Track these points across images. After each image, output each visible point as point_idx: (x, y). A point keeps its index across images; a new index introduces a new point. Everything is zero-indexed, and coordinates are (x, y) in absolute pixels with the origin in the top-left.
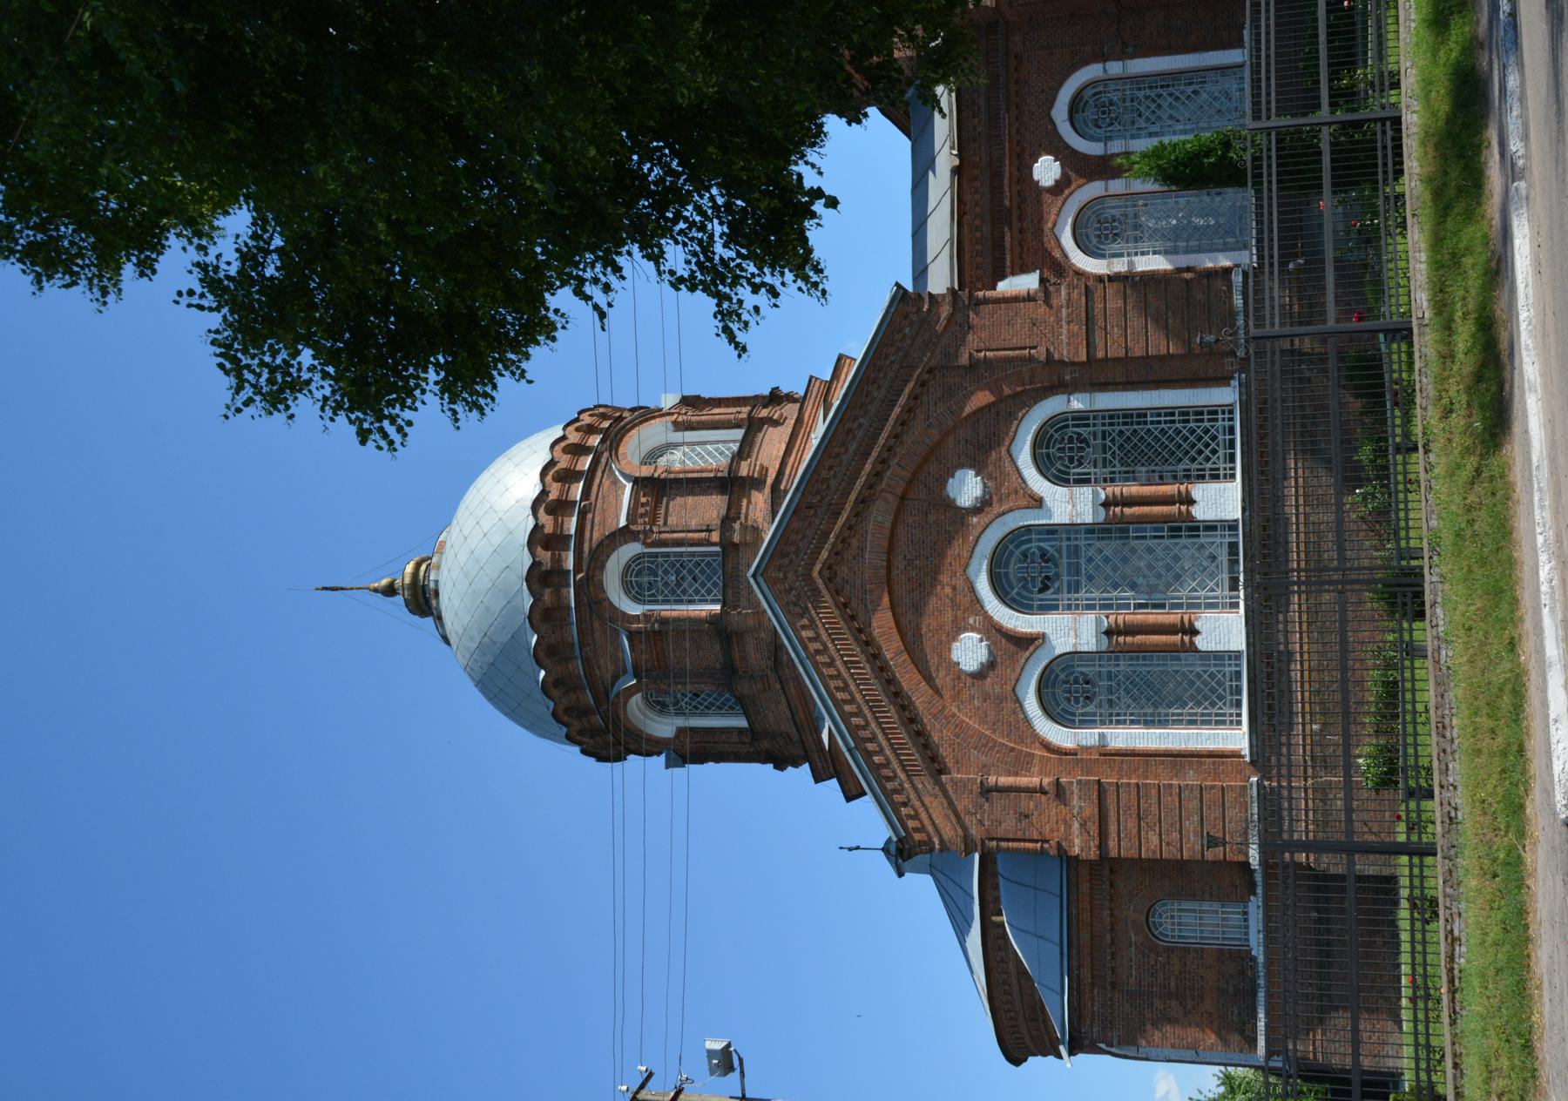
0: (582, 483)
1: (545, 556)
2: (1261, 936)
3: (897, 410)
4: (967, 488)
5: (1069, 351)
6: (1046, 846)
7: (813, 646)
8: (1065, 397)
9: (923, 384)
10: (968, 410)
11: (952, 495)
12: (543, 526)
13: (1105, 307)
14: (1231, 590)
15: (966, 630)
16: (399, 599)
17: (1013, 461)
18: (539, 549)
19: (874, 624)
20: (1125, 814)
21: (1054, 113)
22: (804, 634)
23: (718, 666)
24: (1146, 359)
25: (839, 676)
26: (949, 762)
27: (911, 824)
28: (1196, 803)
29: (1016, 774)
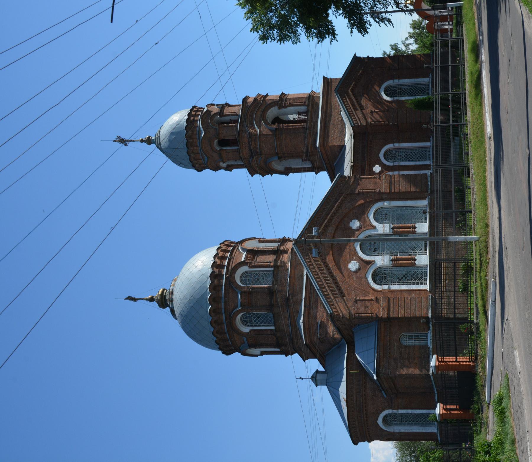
0: (229, 253)
1: (217, 270)
2: (431, 341)
3: (338, 203)
4: (355, 224)
5: (385, 190)
6: (372, 315)
7: (309, 264)
8: (383, 202)
9: (345, 198)
10: (357, 204)
11: (351, 226)
12: (217, 262)
13: (395, 180)
14: (425, 251)
15: (353, 260)
16: (155, 303)
17: (368, 218)
18: (215, 268)
19: (327, 258)
20: (395, 305)
21: (380, 155)
22: (307, 260)
23: (268, 304)
24: (405, 192)
25: (316, 271)
26: (346, 294)
27: (334, 310)
28: (415, 302)
29: (365, 297)
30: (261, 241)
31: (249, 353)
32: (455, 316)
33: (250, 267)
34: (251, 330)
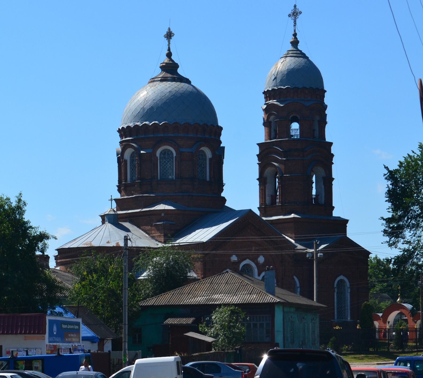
34: (157, 158)
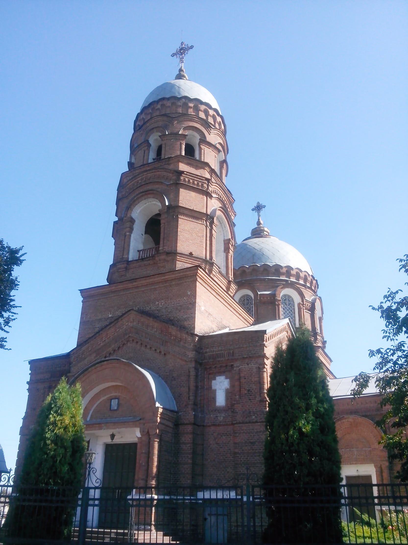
30: (321, 319)
31: (237, 293)
32: (394, 542)
33: (299, 304)
